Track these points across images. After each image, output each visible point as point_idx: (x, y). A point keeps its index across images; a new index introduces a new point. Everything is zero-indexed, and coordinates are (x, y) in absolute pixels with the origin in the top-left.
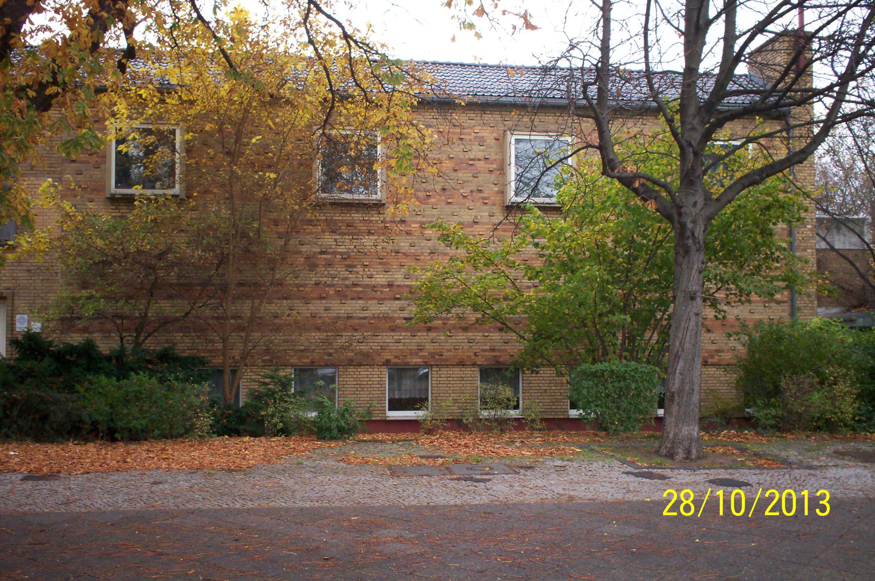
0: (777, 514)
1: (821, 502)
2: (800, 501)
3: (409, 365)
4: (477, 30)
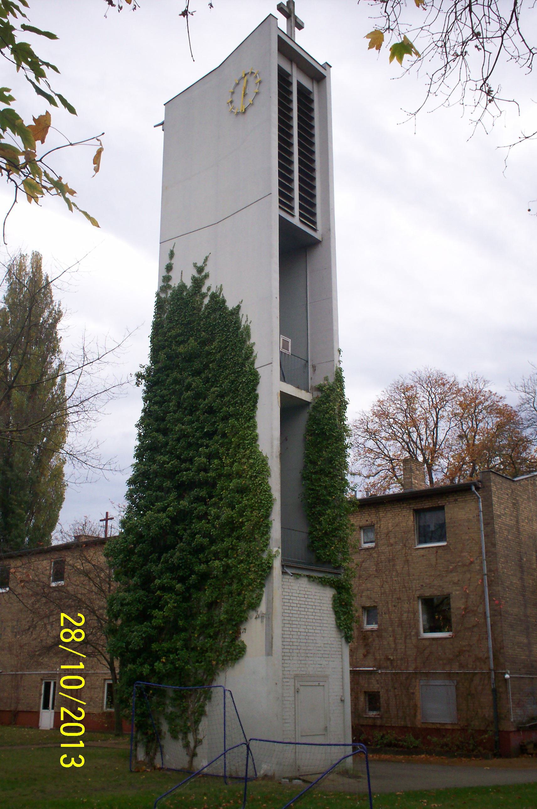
0: (62, 719)
1: (73, 759)
2: (75, 740)
3: (309, 577)
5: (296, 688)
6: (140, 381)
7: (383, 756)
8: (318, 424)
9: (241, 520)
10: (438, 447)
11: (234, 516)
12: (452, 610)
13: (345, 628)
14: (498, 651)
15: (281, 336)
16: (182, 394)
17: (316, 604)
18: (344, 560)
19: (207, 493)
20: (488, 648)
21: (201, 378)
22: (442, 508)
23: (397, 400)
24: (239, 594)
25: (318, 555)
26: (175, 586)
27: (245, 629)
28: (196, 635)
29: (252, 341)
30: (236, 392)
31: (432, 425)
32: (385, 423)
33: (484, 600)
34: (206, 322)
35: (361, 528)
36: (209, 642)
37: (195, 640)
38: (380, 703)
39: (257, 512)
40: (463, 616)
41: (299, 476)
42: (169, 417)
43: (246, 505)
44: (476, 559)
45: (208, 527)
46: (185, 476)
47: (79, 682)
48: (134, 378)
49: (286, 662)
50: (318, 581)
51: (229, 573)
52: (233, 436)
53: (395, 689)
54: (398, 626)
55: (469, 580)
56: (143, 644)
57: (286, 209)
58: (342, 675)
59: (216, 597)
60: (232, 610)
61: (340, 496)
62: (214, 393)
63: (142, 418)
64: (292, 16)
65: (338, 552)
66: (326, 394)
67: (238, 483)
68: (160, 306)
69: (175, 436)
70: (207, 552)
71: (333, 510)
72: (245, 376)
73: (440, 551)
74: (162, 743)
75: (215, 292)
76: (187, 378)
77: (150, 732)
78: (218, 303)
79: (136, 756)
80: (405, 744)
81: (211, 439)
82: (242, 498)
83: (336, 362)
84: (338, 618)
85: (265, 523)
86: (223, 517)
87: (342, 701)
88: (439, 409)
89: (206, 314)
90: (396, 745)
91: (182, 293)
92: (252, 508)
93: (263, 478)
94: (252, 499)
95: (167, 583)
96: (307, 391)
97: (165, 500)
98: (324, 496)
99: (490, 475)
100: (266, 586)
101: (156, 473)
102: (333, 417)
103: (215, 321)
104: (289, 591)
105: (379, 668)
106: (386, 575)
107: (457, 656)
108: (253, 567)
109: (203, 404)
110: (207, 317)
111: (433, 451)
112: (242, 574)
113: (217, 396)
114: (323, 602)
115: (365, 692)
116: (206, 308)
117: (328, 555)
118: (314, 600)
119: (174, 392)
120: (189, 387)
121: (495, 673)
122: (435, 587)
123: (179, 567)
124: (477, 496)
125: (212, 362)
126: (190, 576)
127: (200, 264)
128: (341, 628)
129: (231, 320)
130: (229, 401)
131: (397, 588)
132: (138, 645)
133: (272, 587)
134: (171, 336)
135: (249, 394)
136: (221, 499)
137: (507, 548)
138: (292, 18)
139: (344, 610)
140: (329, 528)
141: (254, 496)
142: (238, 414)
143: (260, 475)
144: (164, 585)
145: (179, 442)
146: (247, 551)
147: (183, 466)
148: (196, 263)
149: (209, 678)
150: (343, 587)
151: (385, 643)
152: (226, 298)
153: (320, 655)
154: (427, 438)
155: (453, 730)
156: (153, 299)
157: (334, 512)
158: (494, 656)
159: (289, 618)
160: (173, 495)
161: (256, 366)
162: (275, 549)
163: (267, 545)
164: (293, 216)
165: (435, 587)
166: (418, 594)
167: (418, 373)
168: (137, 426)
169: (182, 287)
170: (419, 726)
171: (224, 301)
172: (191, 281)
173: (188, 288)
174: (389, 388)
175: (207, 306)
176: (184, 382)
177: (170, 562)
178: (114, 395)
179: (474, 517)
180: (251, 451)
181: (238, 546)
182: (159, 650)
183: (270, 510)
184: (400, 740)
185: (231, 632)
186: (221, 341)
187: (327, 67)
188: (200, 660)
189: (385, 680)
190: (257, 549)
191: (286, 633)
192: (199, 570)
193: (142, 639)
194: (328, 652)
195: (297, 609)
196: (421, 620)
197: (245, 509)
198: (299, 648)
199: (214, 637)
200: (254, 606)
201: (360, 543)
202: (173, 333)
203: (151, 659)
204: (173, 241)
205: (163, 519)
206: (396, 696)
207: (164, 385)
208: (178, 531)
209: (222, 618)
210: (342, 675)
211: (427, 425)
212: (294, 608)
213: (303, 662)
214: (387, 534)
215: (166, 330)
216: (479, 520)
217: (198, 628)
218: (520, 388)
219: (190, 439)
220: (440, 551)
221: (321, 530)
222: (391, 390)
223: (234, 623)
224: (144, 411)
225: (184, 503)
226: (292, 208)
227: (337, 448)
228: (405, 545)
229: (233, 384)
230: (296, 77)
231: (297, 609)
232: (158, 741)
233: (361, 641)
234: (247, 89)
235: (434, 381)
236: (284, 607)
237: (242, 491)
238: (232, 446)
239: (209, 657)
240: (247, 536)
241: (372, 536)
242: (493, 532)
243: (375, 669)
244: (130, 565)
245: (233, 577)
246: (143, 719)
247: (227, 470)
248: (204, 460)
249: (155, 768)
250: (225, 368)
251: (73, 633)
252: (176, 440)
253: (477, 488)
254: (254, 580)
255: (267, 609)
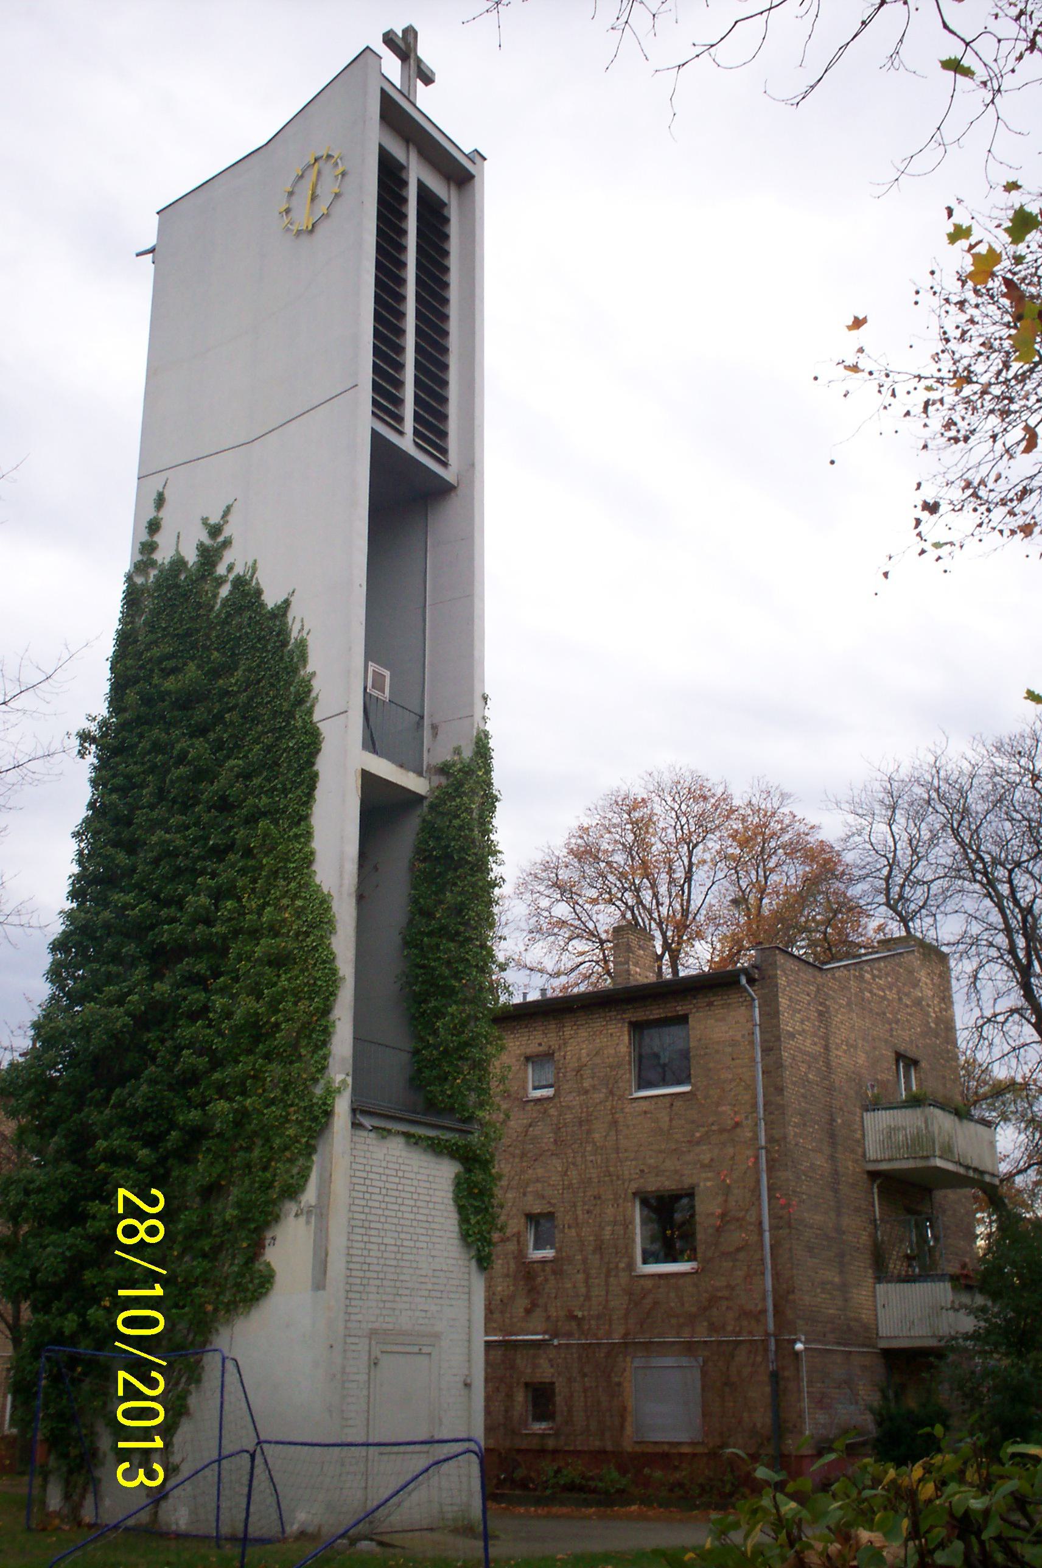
2: (146, 1434)
3: (407, 1135)
5: (373, 1357)
6: (86, 748)
7: (555, 1510)
8: (438, 839)
9: (273, 1019)
10: (690, 917)
11: (260, 1011)
12: (697, 1217)
13: (479, 1240)
14: (783, 1298)
15: (370, 663)
16: (168, 771)
17: (419, 1190)
18: (481, 1105)
19: (210, 968)
20: (765, 1291)
21: (207, 741)
22: (683, 1020)
23: (615, 826)
24: (265, 1169)
25: (430, 1096)
26: (136, 1153)
27: (274, 1239)
28: (176, 1253)
29: (310, 668)
30: (276, 768)
31: (680, 874)
32: (590, 871)
33: (759, 1198)
34: (223, 632)
35: (528, 1059)
36: (199, 1266)
37: (173, 1262)
38: (554, 1404)
39: (307, 1002)
40: (719, 1230)
41: (398, 939)
42: (140, 817)
43: (285, 990)
44: (747, 1118)
45: (208, 1034)
46: (166, 934)
48: (76, 742)
49: (353, 1303)
50: (425, 1144)
51: (247, 1126)
52: (266, 855)
53: (585, 1375)
54: (594, 1252)
55: (733, 1158)
56: (65, 1271)
57: (392, 422)
58: (469, 1334)
59: (219, 1176)
60: (251, 1200)
61: (476, 979)
62: (231, 769)
63: (87, 821)
64: (412, 55)
65: (469, 1089)
66: (456, 779)
67: (270, 946)
68: (132, 600)
69: (150, 855)
70: (204, 1083)
71: (461, 1007)
72: (293, 737)
73: (678, 1103)
74: (98, 1473)
75: (241, 574)
76: (178, 741)
77: (74, 1452)
78: (248, 594)
79: (43, 1503)
80: (600, 1484)
81: (221, 860)
82: (279, 976)
83: (477, 717)
84: (464, 1220)
85: (320, 1026)
86: (239, 1015)
87: (467, 1385)
88: (695, 846)
89: (223, 616)
90: (581, 1489)
91: (177, 576)
92: (295, 996)
93: (322, 936)
94: (297, 977)
95: (120, 1146)
96: (420, 774)
97: (124, 981)
98: (446, 978)
99: (775, 955)
100: (320, 1149)
101: (107, 926)
102: (468, 824)
103: (241, 629)
104: (364, 1161)
105: (555, 1335)
106: (573, 1152)
107: (705, 1309)
108: (295, 1112)
109: (209, 791)
110: (225, 622)
111: (681, 927)
112: (273, 1126)
113: (237, 776)
114: (434, 1186)
115: (527, 1385)
116: (223, 605)
117: (450, 1097)
118: (415, 1183)
119: (153, 769)
120: (182, 759)
121: (777, 1341)
122: (667, 1174)
123: (146, 1115)
124: (750, 995)
125: (230, 710)
126: (168, 1132)
127: (214, 520)
128: (470, 1240)
129: (270, 628)
130: (261, 787)
131: (594, 1176)
132: (55, 1274)
133: (331, 1153)
134: (151, 660)
135: (299, 773)
136: (236, 980)
137: (804, 1096)
138: (412, 61)
139: (476, 1204)
140: (452, 1042)
141: (302, 971)
142: (277, 811)
143: (316, 932)
144: (113, 1152)
145: (158, 866)
146: (284, 1081)
147: (164, 913)
148: (207, 519)
149: (199, 1338)
150: (476, 1159)
151: (569, 1285)
152: (263, 586)
153: (426, 1293)
154: (671, 903)
155: (694, 1455)
156: (119, 588)
157: (464, 1011)
158: (775, 1306)
159: (363, 1217)
160: (140, 972)
161: (316, 717)
162: (339, 1078)
163: (323, 1069)
164: (401, 433)
165: (667, 1174)
166: (633, 1187)
167: (655, 774)
168: (76, 835)
169: (179, 563)
170: (629, 1449)
171: (259, 592)
172: (196, 552)
173: (190, 564)
174: (601, 803)
175: (227, 599)
176: (173, 747)
177: (128, 1104)
178: (36, 776)
179: (743, 1036)
180: (299, 883)
181: (266, 1071)
182: (100, 1283)
183: (332, 998)
184: (592, 1478)
185: (245, 1245)
186: (250, 670)
187: (478, 159)
188: (181, 1304)
189: (565, 1358)
190: (305, 1076)
191: (355, 1245)
192: (185, 1122)
193: (63, 1262)
194: (442, 1288)
195: (380, 1198)
196: (638, 1239)
197: (283, 998)
198: (381, 1275)
199: (212, 1255)
200: (293, 1191)
201: (525, 1089)
202: (156, 652)
203: (82, 1302)
204: (165, 475)
205: (118, 1018)
206: (585, 1390)
207: (133, 755)
208: (148, 1042)
209: (228, 1217)
210: (469, 1334)
211: (671, 871)
212: (374, 1197)
213: (388, 1305)
214: (578, 1071)
215: (143, 647)
216: (752, 1043)
217: (180, 1238)
218: (845, 806)
219: (181, 862)
220: (678, 1103)
221: (436, 1048)
222: (603, 806)
223: (252, 1226)
224: (91, 805)
225: (162, 988)
226: (400, 419)
227: (473, 885)
228: (611, 1093)
229: (269, 752)
230: (417, 172)
231: (380, 1198)
232: (89, 1471)
233: (522, 1283)
234: (319, 187)
235: (686, 791)
236: (354, 1194)
237: (279, 961)
238: (264, 873)
239: (201, 1296)
240: (285, 1051)
241: (549, 1075)
242: (779, 1065)
243: (547, 1337)
244: (48, 1111)
245: (255, 1133)
246: (61, 1425)
247: (251, 920)
248: (204, 900)
249: (79, 1524)
250: (256, 720)
252: (151, 863)
253: (751, 981)
254: (296, 1140)
255: (319, 1196)
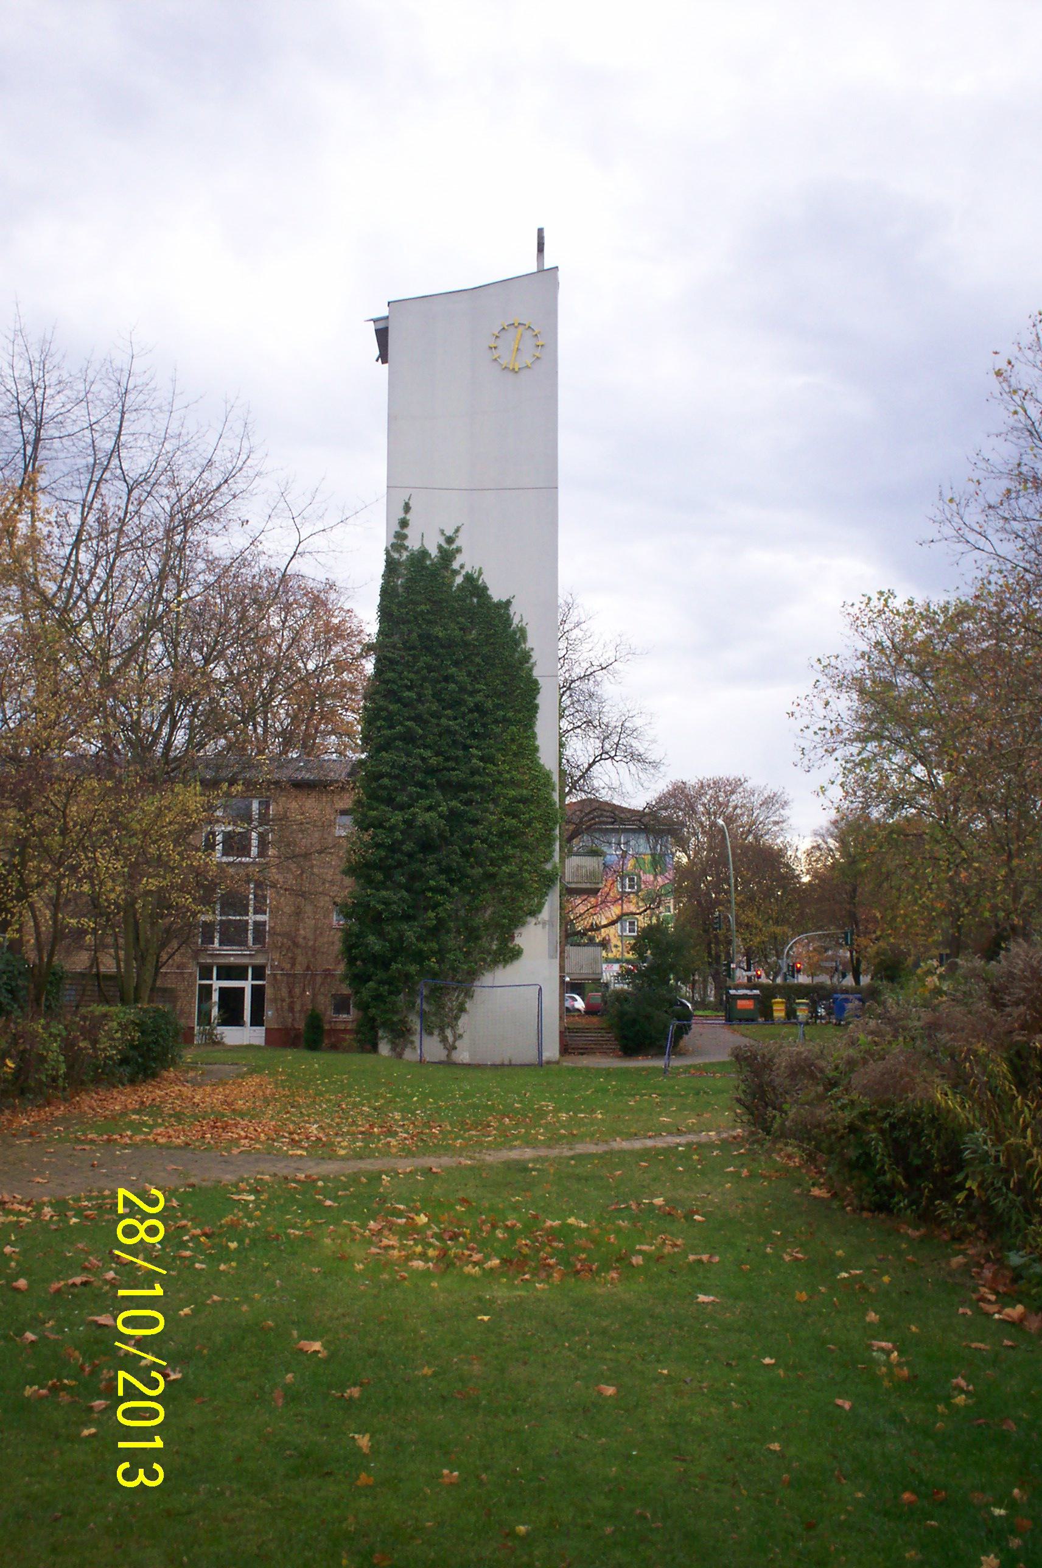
1: (141, 1471)
2: (146, 1434)
4: (398, 529)
47: (153, 1322)
127: (449, 532)
169: (424, 554)
204: (410, 491)
251: (142, 1228)
